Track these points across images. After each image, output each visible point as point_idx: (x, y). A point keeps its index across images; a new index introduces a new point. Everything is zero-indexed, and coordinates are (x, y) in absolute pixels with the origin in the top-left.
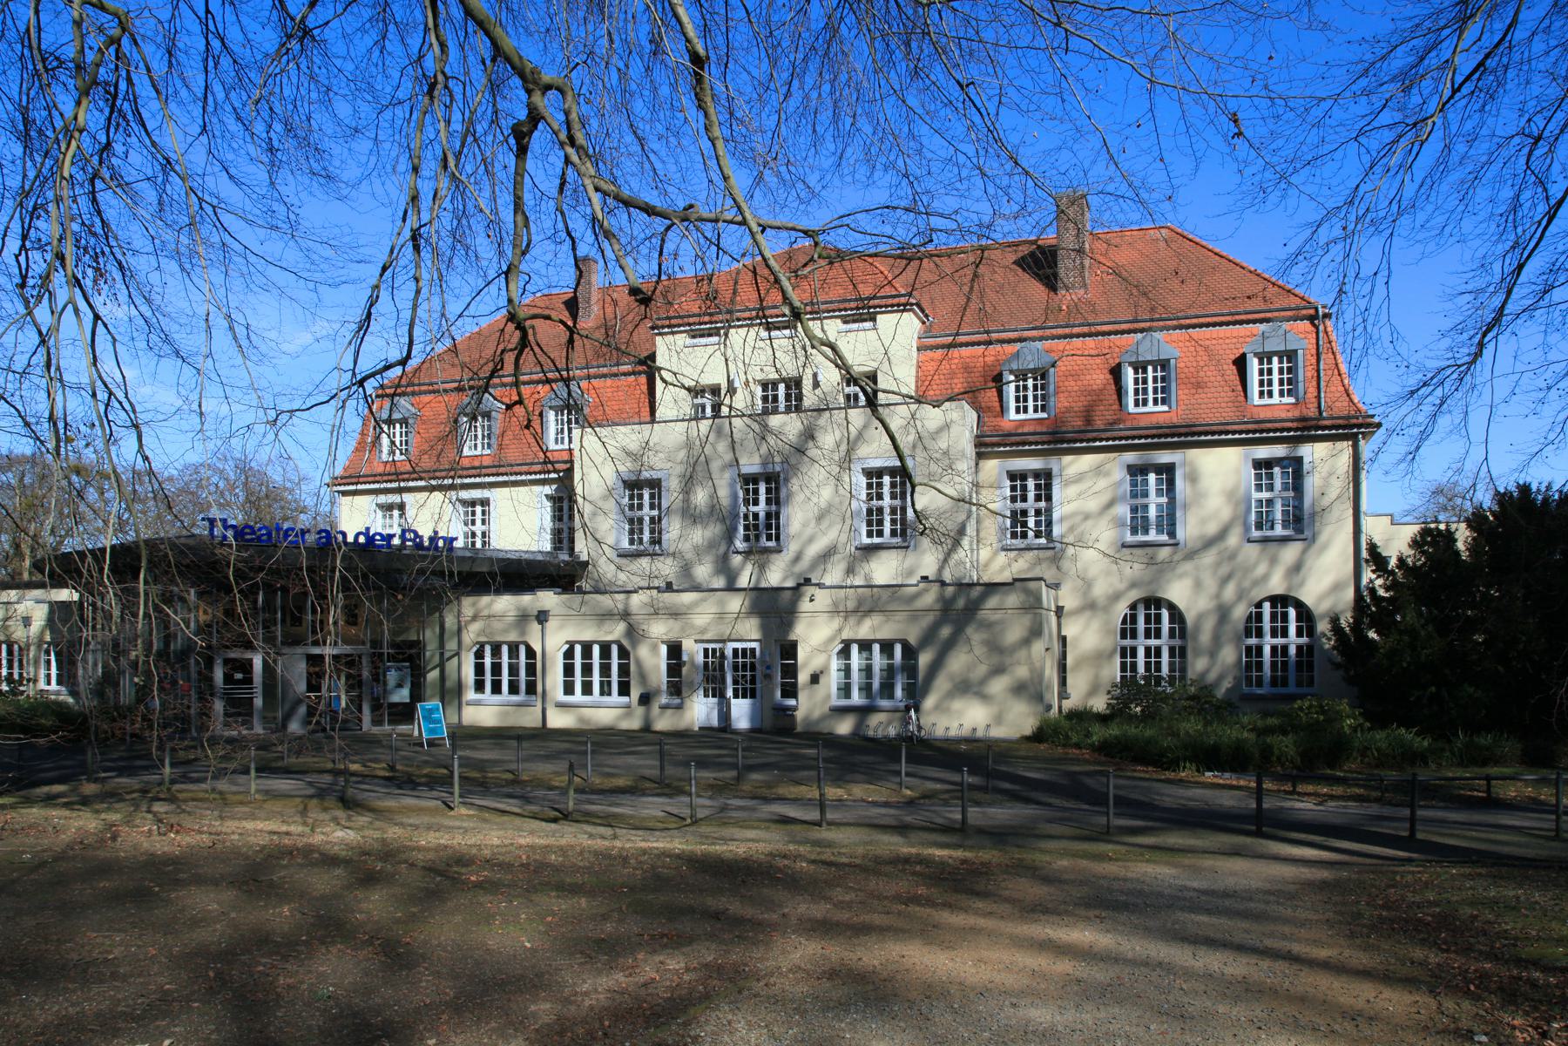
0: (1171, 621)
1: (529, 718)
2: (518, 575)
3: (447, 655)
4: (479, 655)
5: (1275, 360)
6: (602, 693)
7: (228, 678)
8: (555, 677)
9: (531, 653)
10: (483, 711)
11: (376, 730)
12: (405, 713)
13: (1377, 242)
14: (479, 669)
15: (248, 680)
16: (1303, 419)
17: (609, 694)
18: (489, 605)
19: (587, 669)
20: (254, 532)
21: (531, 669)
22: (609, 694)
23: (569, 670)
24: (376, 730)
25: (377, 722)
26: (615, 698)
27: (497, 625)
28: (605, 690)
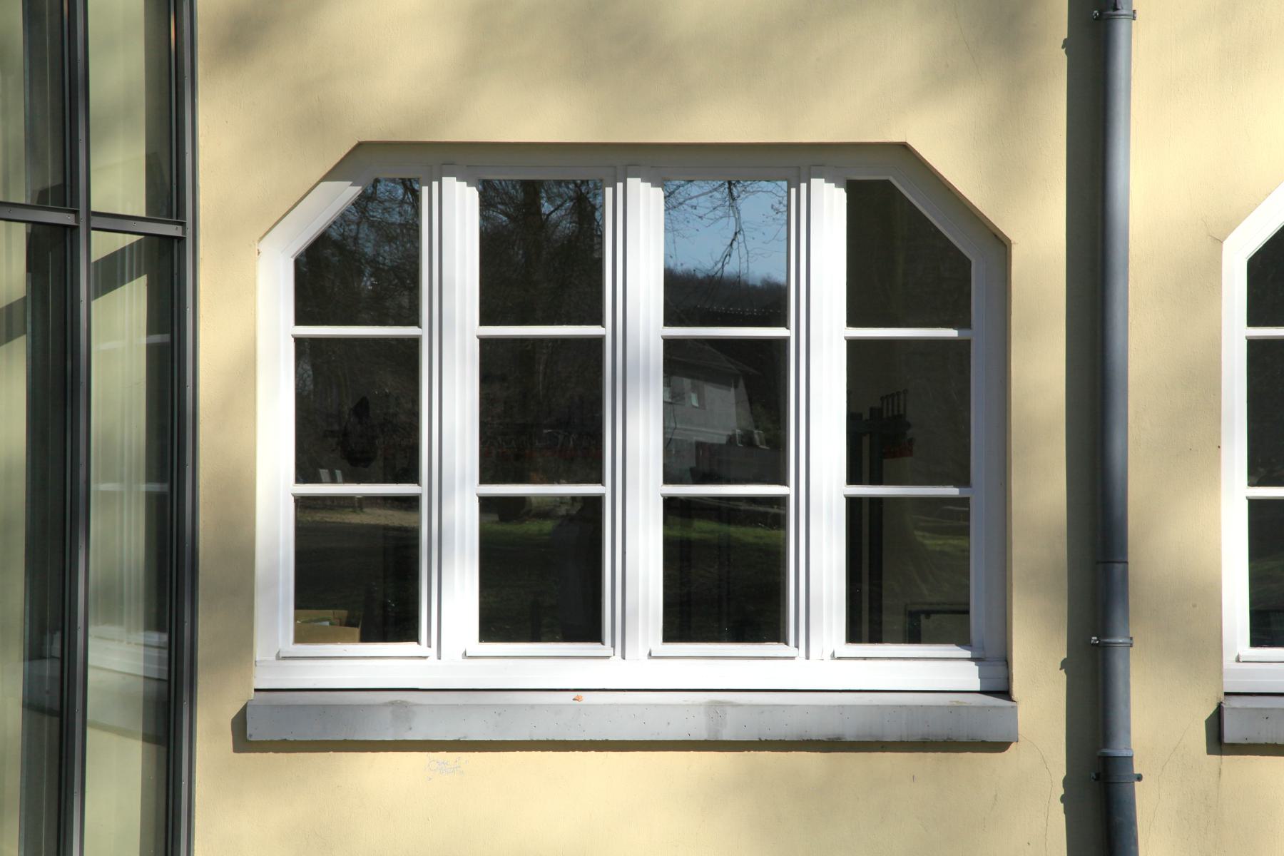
4: (355, 272)
9: (915, 248)
14: (357, 415)
19: (543, 413)
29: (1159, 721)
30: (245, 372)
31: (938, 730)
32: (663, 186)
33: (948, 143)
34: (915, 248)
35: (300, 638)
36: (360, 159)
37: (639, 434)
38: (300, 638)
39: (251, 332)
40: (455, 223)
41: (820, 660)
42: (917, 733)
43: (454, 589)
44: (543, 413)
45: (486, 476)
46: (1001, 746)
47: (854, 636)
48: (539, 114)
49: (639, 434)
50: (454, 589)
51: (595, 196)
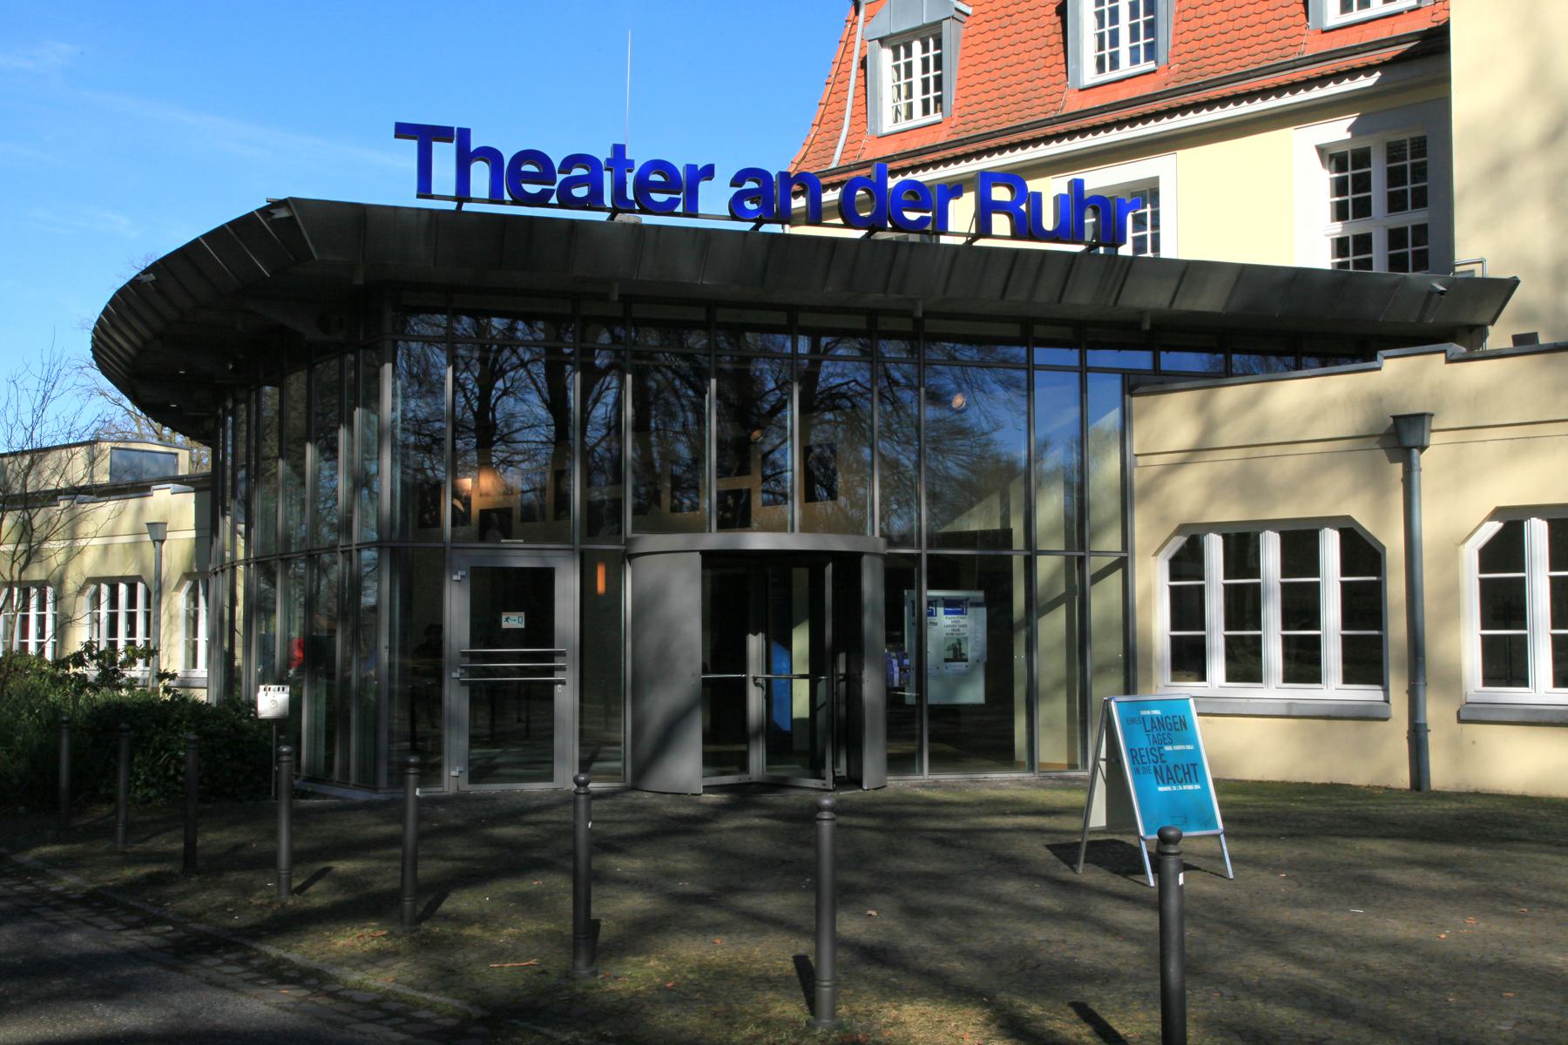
0: (1349, 564)
1: (1380, 762)
2: (1269, 325)
3: (1095, 564)
4: (1187, 562)
5: (917, 46)
6: (1289, 677)
7: (485, 628)
8: (1464, 643)
9: (1361, 553)
10: (1250, 731)
11: (898, 784)
12: (982, 736)
13: (856, 353)
14: (1187, 608)
15: (541, 627)
16: (91, 624)
17: (1315, 677)
18: (1253, 402)
19: (1243, 608)
20: (546, 174)
21: (1363, 606)
22: (1315, 677)
23: (1503, 605)
24: (898, 784)
25: (900, 763)
26: (1274, 689)
27: (1286, 466)
28: (1303, 662)
29: (1437, 712)
30: (1149, 594)
31: (1362, 713)
32: (748, 371)
33: (1365, 521)
34: (1361, 553)
35: (1173, 679)
36: (1182, 529)
37: (1272, 613)
38: (1173, 679)
39: (1153, 582)
40: (1214, 549)
41: (1274, 689)
42: (1322, 713)
43: (1217, 666)
44: (1243, 608)
45: (1228, 628)
46: (1386, 719)
47: (1526, 685)
48: (1232, 513)
49: (1272, 613)
50: (1217, 666)
51: (999, 461)
